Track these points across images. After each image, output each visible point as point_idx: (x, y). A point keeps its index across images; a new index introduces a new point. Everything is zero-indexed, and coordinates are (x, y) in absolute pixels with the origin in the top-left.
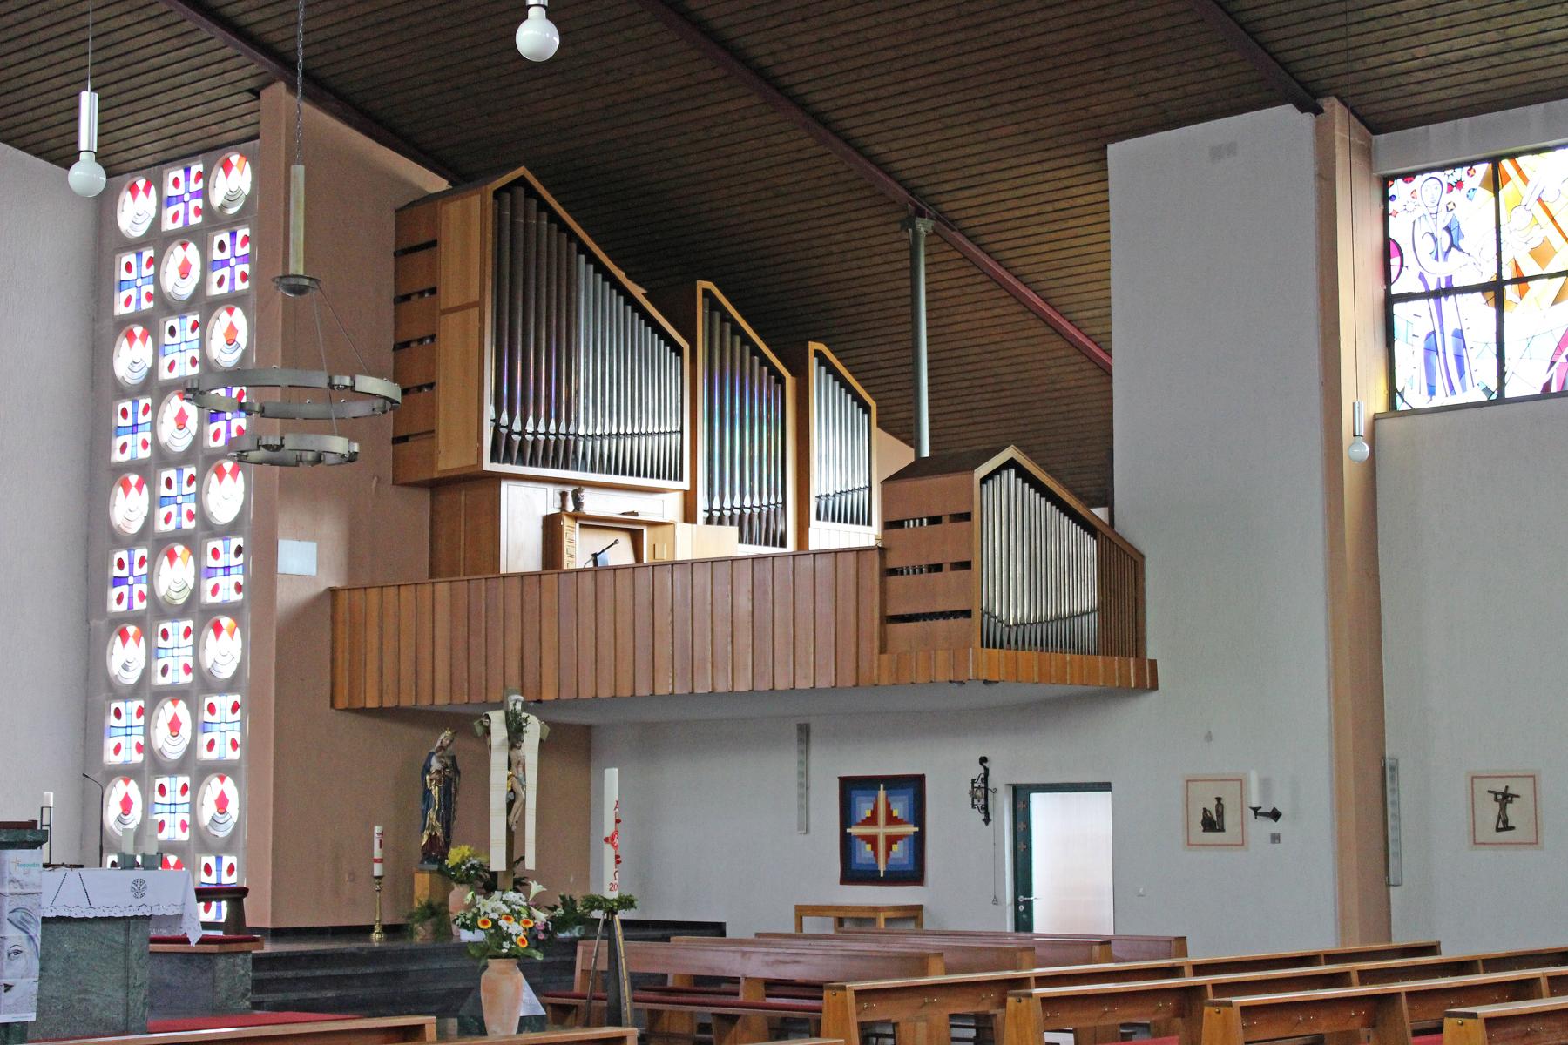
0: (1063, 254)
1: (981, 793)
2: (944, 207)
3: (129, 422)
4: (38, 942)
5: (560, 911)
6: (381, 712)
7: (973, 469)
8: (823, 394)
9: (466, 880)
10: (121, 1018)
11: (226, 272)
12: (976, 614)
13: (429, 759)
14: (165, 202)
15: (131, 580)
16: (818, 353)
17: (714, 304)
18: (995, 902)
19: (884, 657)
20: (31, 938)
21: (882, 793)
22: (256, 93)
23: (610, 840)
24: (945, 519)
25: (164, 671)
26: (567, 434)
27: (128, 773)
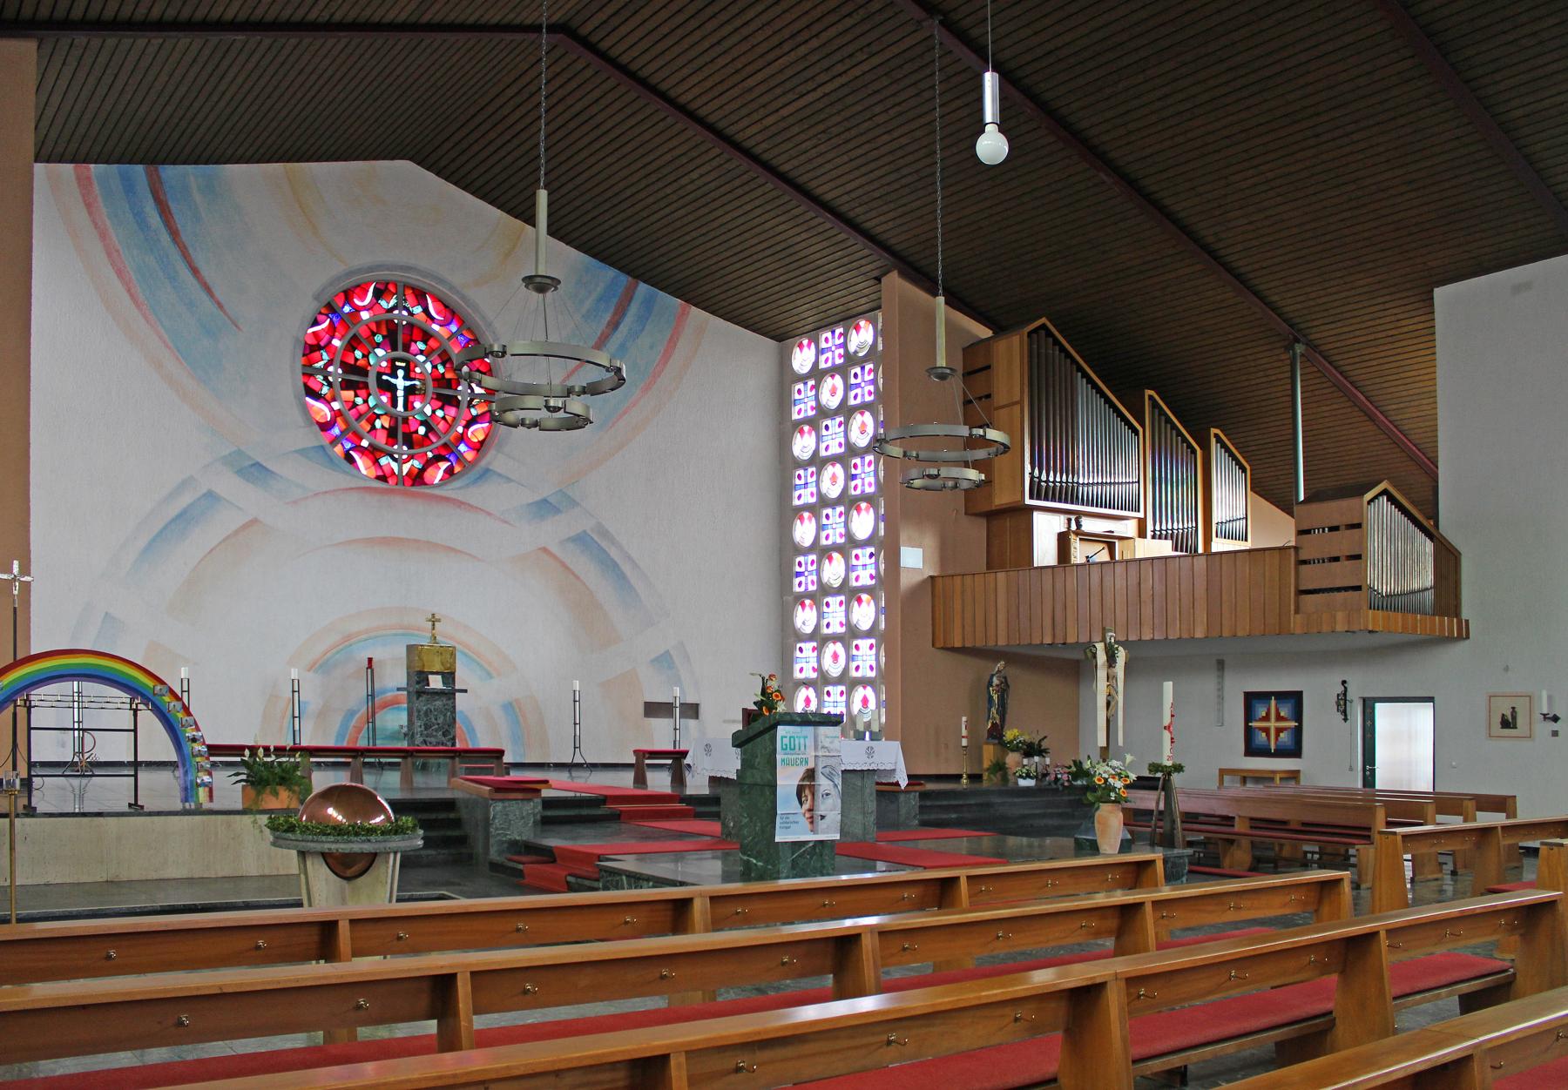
0: (1387, 366)
1: (1342, 703)
2: (1312, 337)
3: (802, 482)
4: (840, 787)
5: (1074, 769)
6: (962, 650)
7: (1363, 494)
8: (1219, 461)
9: (1016, 749)
10: (861, 832)
11: (859, 391)
12: (1364, 589)
13: (992, 676)
14: (820, 352)
15: (806, 574)
16: (1216, 436)
17: (1155, 405)
18: (1351, 769)
19: (1298, 616)
20: (836, 786)
21: (1273, 702)
22: (878, 279)
23: (1167, 728)
24: (1342, 528)
25: (828, 625)
26: (1073, 482)
27: (807, 683)
